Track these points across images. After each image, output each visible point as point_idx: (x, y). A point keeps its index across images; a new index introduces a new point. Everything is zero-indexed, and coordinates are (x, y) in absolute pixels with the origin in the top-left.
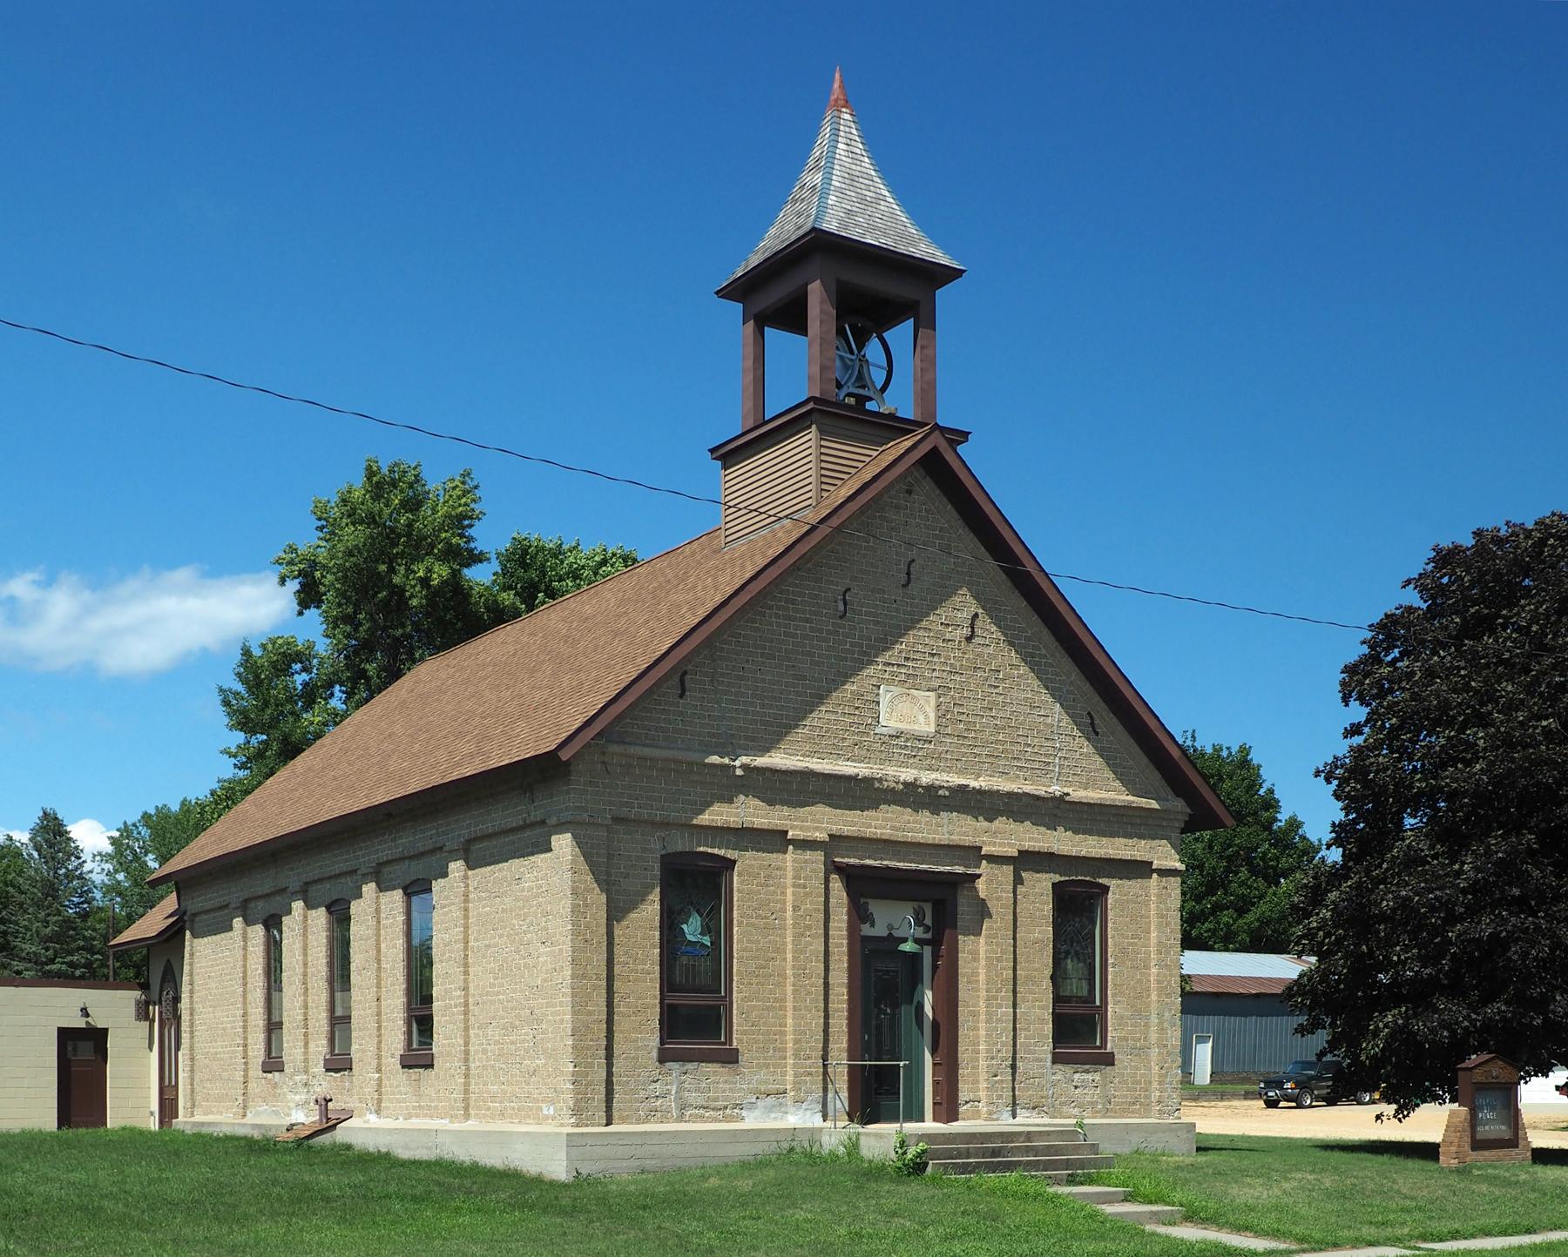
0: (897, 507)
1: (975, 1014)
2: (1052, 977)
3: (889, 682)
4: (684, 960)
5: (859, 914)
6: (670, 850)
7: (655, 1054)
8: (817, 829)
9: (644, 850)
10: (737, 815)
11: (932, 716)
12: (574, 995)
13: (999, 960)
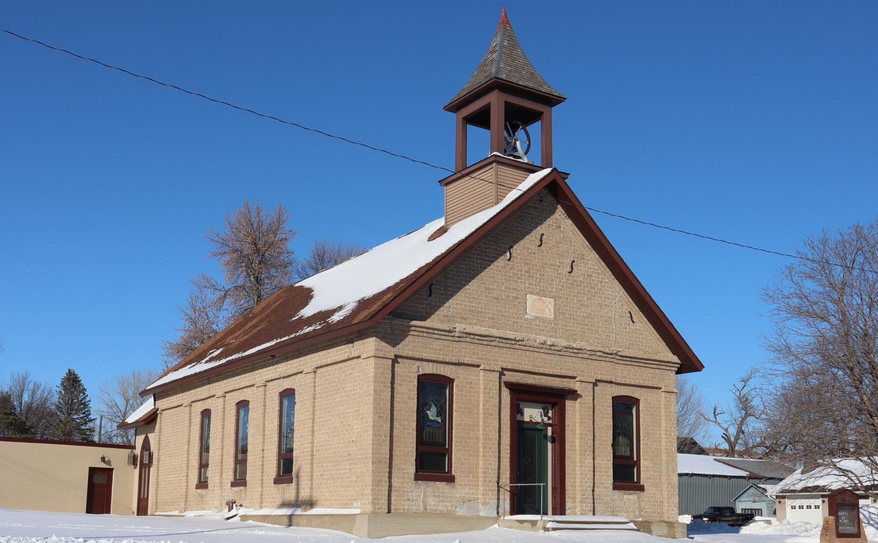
0: (535, 208)
1: (574, 462)
2: (613, 445)
3: (531, 293)
4: (428, 429)
5: (516, 410)
6: (421, 373)
7: (413, 476)
8: (495, 365)
9: (410, 372)
10: (456, 356)
11: (552, 310)
12: (373, 444)
13: (586, 435)
